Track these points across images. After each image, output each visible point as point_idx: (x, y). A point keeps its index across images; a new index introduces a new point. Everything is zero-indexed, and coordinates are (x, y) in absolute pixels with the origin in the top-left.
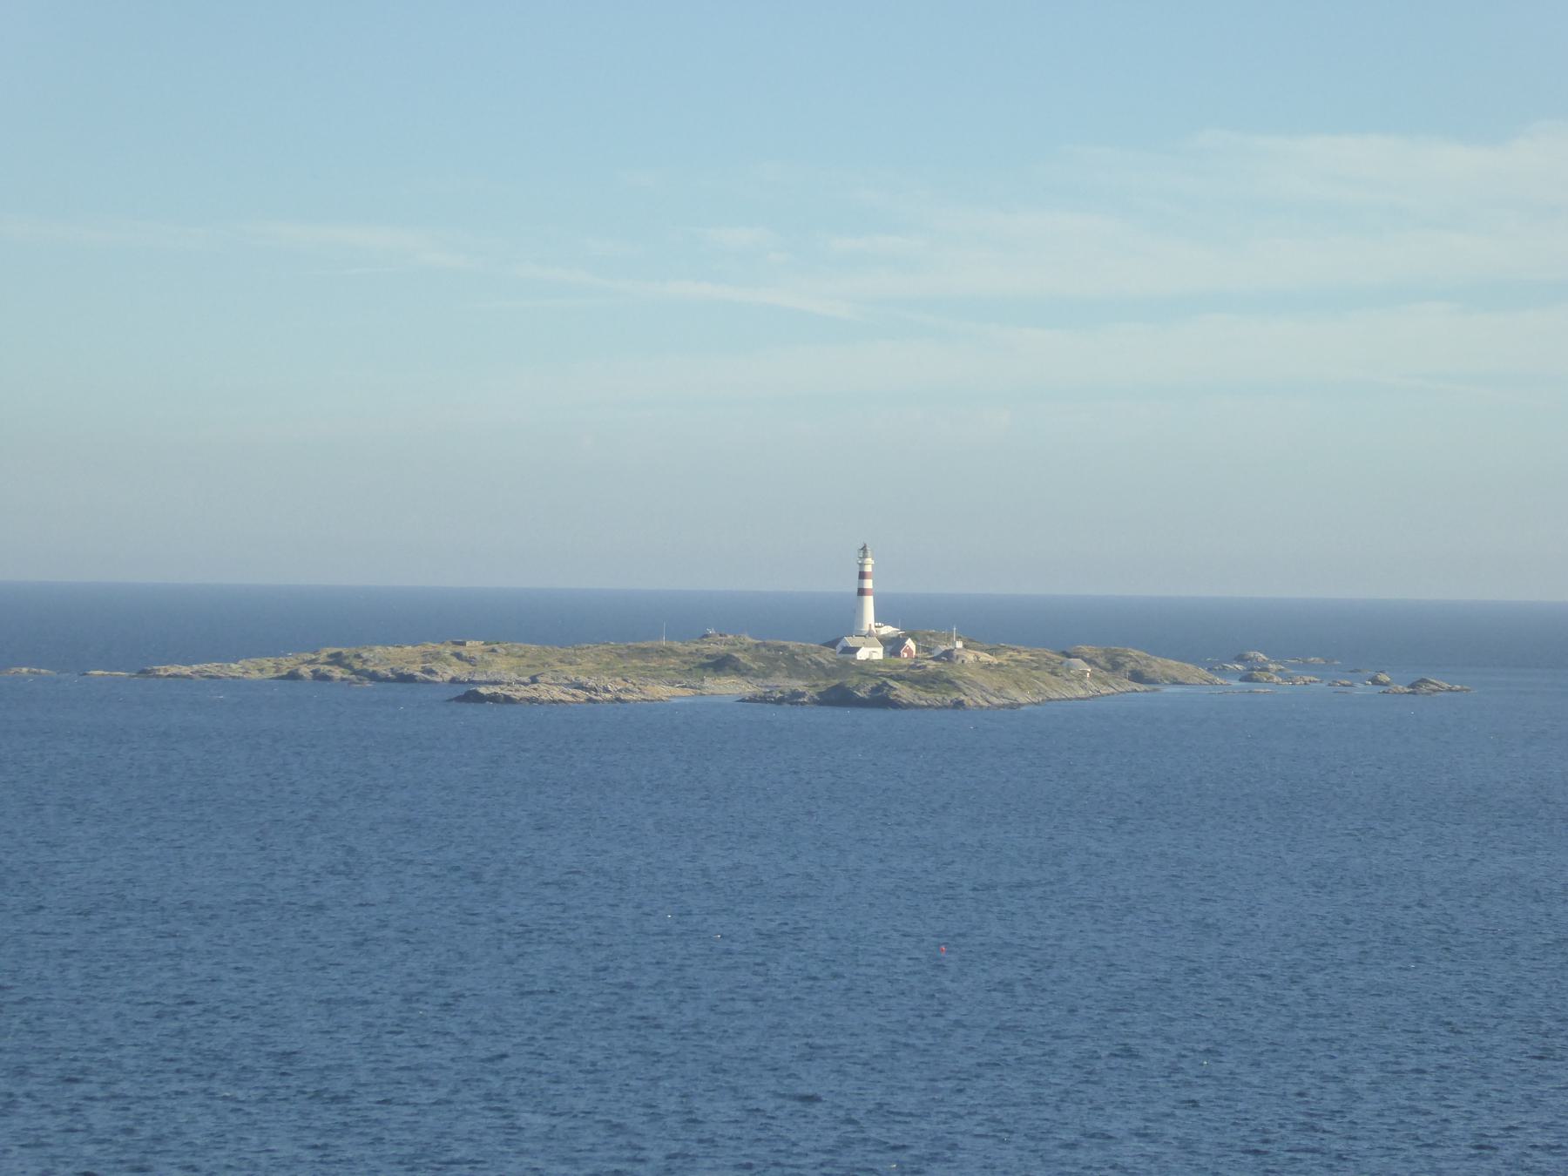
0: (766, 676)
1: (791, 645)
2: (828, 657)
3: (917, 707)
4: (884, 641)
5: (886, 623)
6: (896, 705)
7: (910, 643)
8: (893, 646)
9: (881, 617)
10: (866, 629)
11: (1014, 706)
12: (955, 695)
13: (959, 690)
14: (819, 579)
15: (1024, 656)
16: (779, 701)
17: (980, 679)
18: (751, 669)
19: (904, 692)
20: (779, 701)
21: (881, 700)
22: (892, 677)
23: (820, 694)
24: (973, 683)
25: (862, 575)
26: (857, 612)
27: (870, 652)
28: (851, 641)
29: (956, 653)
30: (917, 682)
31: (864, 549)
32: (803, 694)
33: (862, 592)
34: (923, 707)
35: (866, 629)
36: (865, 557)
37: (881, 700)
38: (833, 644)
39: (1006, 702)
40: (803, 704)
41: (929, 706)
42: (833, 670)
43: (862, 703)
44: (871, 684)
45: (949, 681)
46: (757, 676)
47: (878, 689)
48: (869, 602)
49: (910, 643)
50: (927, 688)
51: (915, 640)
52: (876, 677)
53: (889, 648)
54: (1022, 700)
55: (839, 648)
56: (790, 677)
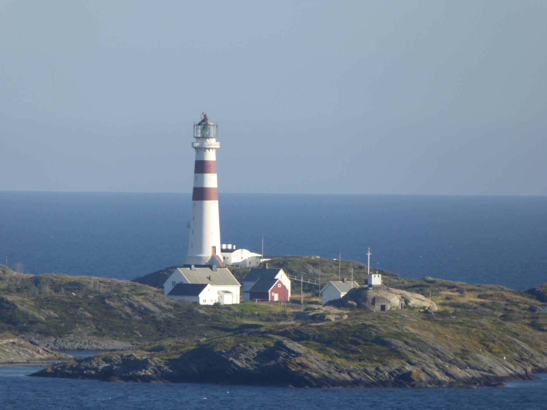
0: (60, 333)
1: (92, 281)
2: (156, 301)
3: (335, 383)
4: (240, 273)
5: (32, 274)
6: (300, 380)
7: (283, 278)
8: (256, 282)
9: (231, 235)
10: (207, 254)
11: (491, 381)
12: (395, 364)
13: (399, 355)
14: (140, 174)
15: (470, 298)
16: (105, 376)
17: (429, 337)
18: (34, 322)
19: (313, 360)
20: (105, 376)
21: (274, 372)
22: (285, 334)
23: (171, 363)
24: (420, 345)
25: (201, 167)
26: (194, 226)
27: (220, 294)
28: (189, 275)
29: (371, 294)
30: (329, 343)
31: (204, 124)
32: (144, 364)
33: (200, 194)
34: (344, 383)
35: (207, 254)
36: (204, 137)
37: (274, 372)
38: (156, 279)
39: (476, 374)
40: (146, 379)
41: (356, 383)
42: (168, 322)
43: (242, 378)
44: (257, 346)
45: (380, 341)
46: (45, 333)
47: (268, 354)
48: (212, 210)
49: (283, 278)
50: (347, 352)
51: (289, 272)
52: (264, 335)
53: (250, 285)
54: (501, 371)
55: (168, 286)
56: (99, 334)
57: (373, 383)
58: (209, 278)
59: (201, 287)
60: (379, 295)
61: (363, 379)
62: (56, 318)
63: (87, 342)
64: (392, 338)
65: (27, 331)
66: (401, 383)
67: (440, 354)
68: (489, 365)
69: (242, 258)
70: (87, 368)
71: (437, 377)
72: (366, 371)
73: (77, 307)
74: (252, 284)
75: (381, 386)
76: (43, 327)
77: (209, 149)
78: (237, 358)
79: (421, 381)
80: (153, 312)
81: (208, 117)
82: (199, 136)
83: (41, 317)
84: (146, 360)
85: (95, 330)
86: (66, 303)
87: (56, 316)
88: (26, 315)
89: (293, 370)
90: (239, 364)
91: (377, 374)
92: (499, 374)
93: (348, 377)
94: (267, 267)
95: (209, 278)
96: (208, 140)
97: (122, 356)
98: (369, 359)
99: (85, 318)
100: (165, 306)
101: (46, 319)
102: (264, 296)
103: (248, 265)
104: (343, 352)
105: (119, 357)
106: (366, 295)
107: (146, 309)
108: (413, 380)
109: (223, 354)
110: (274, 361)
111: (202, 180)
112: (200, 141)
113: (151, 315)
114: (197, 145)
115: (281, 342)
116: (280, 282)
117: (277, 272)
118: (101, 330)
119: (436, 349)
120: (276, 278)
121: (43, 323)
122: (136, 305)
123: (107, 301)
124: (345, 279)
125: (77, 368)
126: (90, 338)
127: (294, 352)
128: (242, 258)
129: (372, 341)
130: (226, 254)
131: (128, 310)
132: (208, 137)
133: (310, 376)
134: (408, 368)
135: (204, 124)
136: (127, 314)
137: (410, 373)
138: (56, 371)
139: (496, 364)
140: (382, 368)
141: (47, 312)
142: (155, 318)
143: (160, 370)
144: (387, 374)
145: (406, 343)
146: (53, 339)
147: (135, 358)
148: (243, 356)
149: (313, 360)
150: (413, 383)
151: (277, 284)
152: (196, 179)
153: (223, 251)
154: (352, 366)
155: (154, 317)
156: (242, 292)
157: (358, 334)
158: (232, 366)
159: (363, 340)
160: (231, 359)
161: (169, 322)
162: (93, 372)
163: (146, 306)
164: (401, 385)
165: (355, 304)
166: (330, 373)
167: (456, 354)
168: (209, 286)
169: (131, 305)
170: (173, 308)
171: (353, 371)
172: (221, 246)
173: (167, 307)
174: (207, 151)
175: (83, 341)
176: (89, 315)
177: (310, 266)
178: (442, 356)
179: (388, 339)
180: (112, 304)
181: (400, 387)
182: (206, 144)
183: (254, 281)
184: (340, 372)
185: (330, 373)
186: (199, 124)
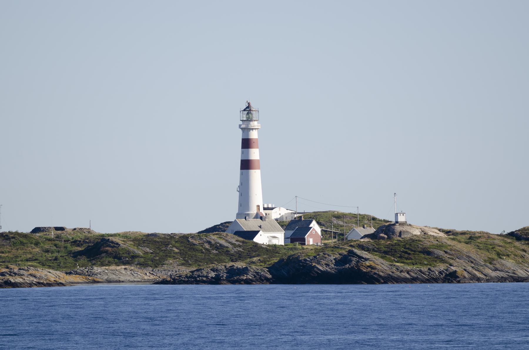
12: (442, 267)
30: (386, 253)
31: (248, 109)
47: (344, 260)
57: (428, 280)
58: (260, 227)
59: (256, 233)
60: (404, 230)
61: (419, 277)
62: (152, 253)
63: (177, 270)
64: (435, 248)
65: (129, 263)
66: (449, 279)
67: (473, 261)
68: (512, 268)
69: (280, 214)
70: (199, 276)
71: (476, 275)
72: (421, 271)
73: (168, 244)
74: (291, 232)
75: (433, 281)
76: (142, 260)
77: (253, 129)
78: (319, 263)
79: (465, 277)
80: (227, 247)
81: (252, 105)
82: (245, 119)
83: (140, 253)
84: (247, 267)
85: (183, 262)
86: (158, 242)
87: (151, 251)
88: (129, 252)
89: (365, 271)
90: (321, 268)
91: (429, 273)
92: (520, 275)
93: (408, 276)
94: (303, 219)
95: (260, 227)
96: (251, 123)
97: (225, 267)
98: (421, 263)
99: (174, 253)
100: (235, 242)
101: (144, 254)
102: (302, 241)
103: (285, 220)
104: (399, 259)
105: (223, 267)
106: (394, 229)
107: (221, 245)
108: (459, 277)
109: (308, 261)
110: (348, 265)
111: (248, 154)
112: (246, 123)
113: (225, 249)
114: (243, 126)
115: (352, 251)
116: (314, 229)
117: (311, 222)
118: (187, 261)
119: (469, 257)
120: (310, 226)
121: (142, 257)
122: (213, 242)
123: (190, 240)
124: (365, 226)
125: (191, 277)
126: (180, 267)
127: (363, 258)
128: (280, 214)
129: (420, 252)
130: (268, 212)
131: (207, 246)
132: (251, 120)
133: (379, 275)
134: (453, 268)
135: (248, 109)
136: (207, 249)
137: (456, 271)
138: (174, 279)
139: (517, 268)
140: (433, 269)
141: (144, 249)
142: (229, 251)
143: (258, 275)
144: (437, 273)
145: (446, 252)
146: (151, 269)
147: (237, 267)
148: (323, 262)
149: (379, 263)
150: (458, 279)
151: (311, 232)
152: (243, 153)
153: (265, 209)
154: (409, 268)
155: (227, 251)
156: (286, 238)
157: (407, 246)
158: (315, 269)
159: (412, 251)
160: (314, 264)
161: (240, 254)
162: (205, 279)
163: (221, 243)
164: (450, 282)
165: (386, 236)
166: (393, 273)
167: (485, 261)
168: (261, 233)
169: (209, 243)
170: (241, 244)
171: (411, 271)
172: (264, 205)
173: (237, 243)
174: (251, 131)
175: (174, 270)
176: (176, 250)
177: (335, 219)
178: (474, 262)
179: (431, 250)
180: (194, 242)
181: (449, 282)
182: (250, 126)
183: (293, 230)
184: (401, 272)
185: (393, 273)
186: (245, 110)
